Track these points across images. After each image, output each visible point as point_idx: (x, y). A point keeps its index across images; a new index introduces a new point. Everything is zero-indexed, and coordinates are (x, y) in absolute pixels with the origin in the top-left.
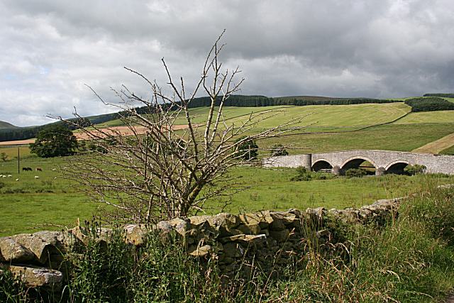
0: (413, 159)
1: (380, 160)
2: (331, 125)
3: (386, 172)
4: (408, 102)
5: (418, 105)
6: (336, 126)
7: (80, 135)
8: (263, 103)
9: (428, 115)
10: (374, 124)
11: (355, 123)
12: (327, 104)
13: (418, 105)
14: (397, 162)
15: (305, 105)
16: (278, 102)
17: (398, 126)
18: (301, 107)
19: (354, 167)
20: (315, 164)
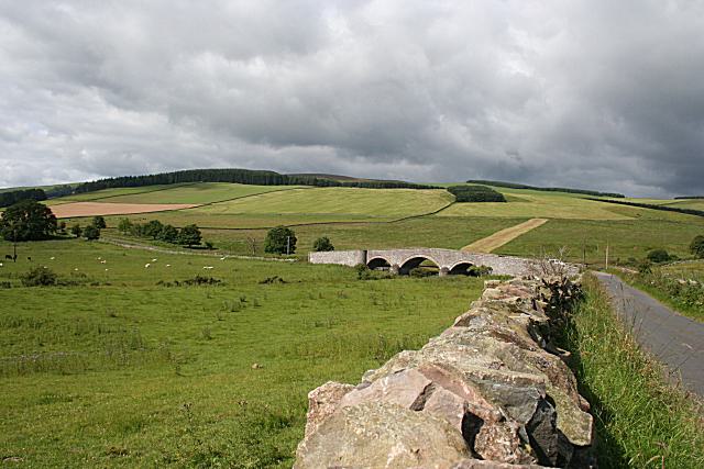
1: (444, 260)
3: (449, 273)
4: (450, 190)
5: (462, 194)
7: (60, 210)
8: (275, 182)
9: (474, 207)
10: (413, 214)
13: (462, 194)
17: (441, 218)
18: (323, 189)
19: (412, 267)
20: (371, 261)
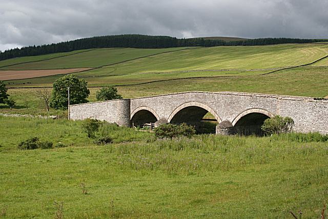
0: (277, 107)
1: (225, 109)
2: (237, 68)
6: (244, 70)
11: (266, 65)
12: (239, 45)
14: (249, 112)
15: (214, 46)
16: (253, 42)
17: (317, 68)
